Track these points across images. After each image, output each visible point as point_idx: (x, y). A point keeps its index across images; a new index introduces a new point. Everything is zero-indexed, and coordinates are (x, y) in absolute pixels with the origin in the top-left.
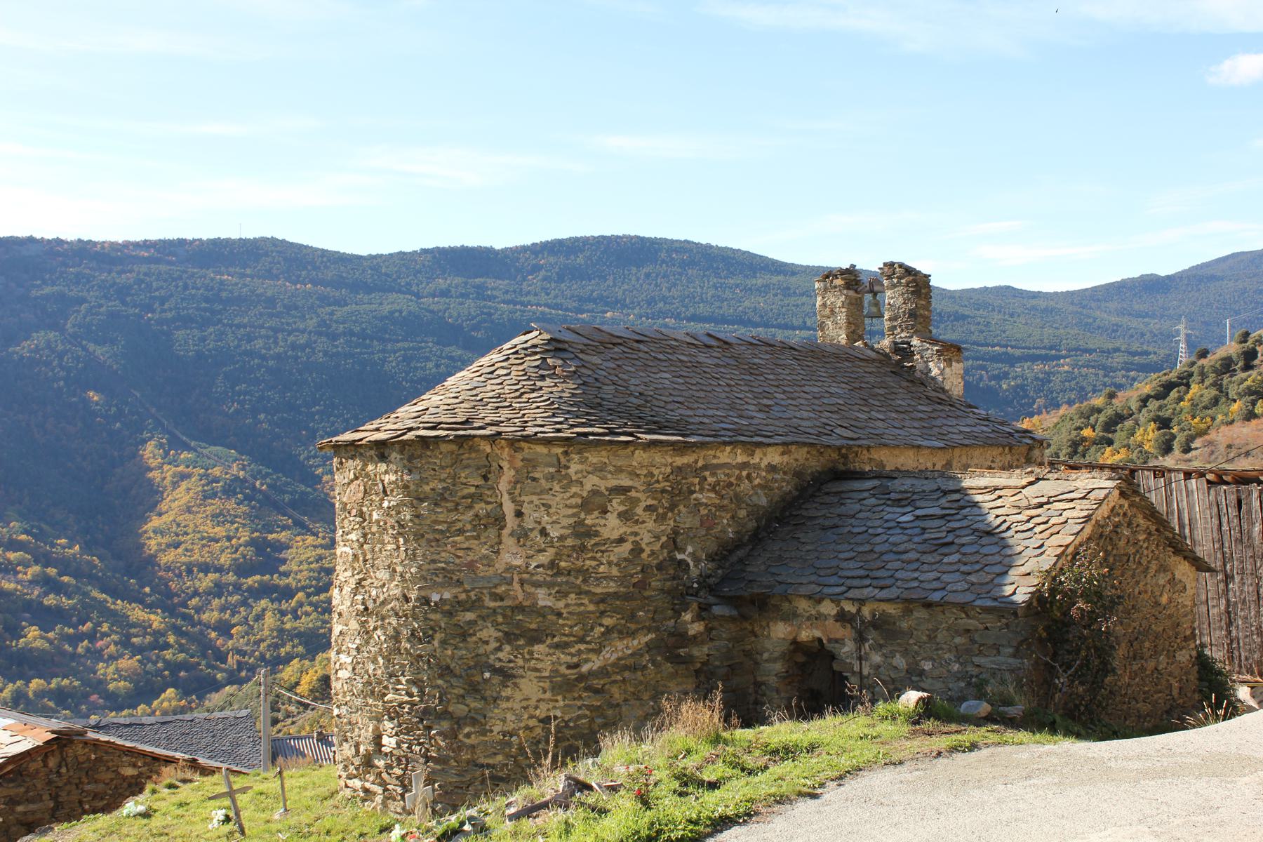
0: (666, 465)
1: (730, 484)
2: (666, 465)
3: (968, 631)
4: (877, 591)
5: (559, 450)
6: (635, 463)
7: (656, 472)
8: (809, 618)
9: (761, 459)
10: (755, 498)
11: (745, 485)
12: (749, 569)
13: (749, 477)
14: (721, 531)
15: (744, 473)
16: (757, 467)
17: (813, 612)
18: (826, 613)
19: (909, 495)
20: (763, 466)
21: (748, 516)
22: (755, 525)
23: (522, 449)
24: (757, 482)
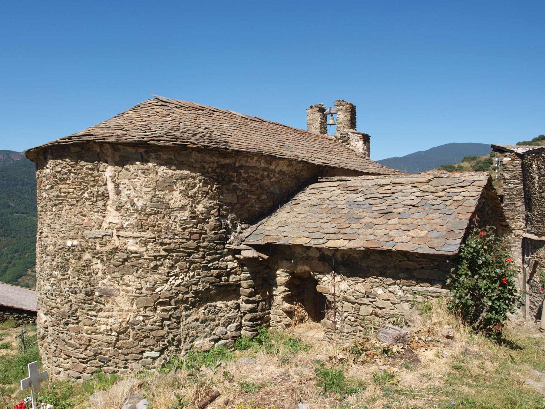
0: (213, 163)
1: (257, 179)
2: (213, 163)
3: (408, 269)
4: (346, 242)
5: (142, 150)
6: (192, 160)
7: (207, 166)
8: (302, 259)
9: (276, 167)
10: (272, 189)
11: (266, 181)
12: (267, 228)
13: (268, 176)
14: (250, 206)
15: (266, 174)
16: (273, 171)
17: (305, 255)
18: (313, 255)
19: (359, 188)
20: (277, 171)
21: (268, 198)
22: (272, 204)
23: (120, 150)
24: (273, 179)
